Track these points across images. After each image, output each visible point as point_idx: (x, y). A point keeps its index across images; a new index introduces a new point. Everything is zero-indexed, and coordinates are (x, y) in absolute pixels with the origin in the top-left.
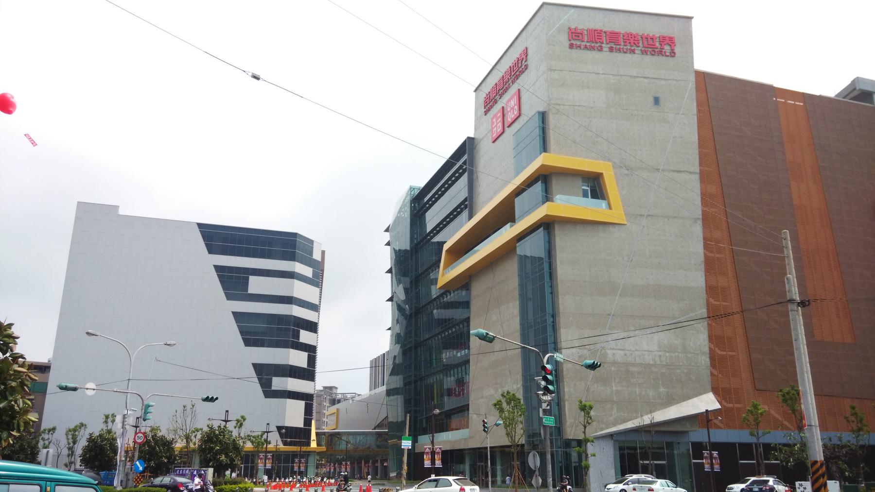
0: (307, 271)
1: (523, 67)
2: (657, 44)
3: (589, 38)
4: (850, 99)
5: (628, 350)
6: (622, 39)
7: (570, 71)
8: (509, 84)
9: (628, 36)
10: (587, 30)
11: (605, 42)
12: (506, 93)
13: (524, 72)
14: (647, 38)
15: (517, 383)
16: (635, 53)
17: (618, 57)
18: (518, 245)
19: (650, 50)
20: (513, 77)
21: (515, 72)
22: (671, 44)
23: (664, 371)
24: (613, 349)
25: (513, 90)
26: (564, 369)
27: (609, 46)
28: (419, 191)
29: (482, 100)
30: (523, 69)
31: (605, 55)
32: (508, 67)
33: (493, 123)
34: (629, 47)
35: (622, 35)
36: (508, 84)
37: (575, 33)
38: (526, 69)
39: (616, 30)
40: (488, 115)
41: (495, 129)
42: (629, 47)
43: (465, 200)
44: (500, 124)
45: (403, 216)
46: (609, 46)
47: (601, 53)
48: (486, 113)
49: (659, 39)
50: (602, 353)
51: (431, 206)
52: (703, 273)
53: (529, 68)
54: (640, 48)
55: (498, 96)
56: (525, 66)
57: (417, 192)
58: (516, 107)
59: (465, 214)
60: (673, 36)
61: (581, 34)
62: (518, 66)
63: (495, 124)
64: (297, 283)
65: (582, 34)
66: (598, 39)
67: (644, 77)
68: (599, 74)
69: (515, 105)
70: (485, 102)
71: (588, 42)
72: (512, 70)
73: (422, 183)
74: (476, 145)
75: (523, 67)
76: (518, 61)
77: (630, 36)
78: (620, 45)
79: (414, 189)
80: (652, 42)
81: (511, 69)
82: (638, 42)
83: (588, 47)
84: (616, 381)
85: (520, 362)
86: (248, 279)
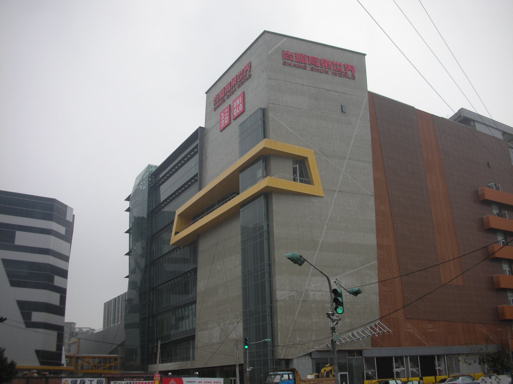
0: (62, 230)
1: (248, 75)
2: (343, 70)
3: (297, 59)
4: (458, 122)
5: (325, 292)
6: (319, 64)
7: (284, 81)
8: (235, 88)
9: (324, 62)
10: (295, 54)
11: (308, 64)
12: (233, 95)
13: (248, 79)
14: (336, 65)
15: (237, 318)
16: (328, 74)
17: (317, 75)
18: (241, 210)
19: (339, 73)
20: (239, 83)
21: (240, 79)
22: (352, 70)
23: (349, 306)
24: (314, 291)
25: (239, 92)
26: (278, 306)
27: (310, 66)
28: (155, 169)
29: (212, 99)
30: (247, 77)
31: (308, 72)
32: (235, 76)
33: (221, 117)
34: (324, 69)
35: (319, 60)
36: (234, 88)
37: (287, 55)
38: (250, 77)
39: (315, 56)
40: (217, 110)
41: (223, 121)
42: (324, 69)
43: (196, 175)
44: (227, 117)
45: (141, 188)
46: (310, 66)
47: (305, 71)
48: (215, 109)
49: (344, 66)
50: (306, 293)
51: (165, 180)
52: (375, 235)
53: (252, 77)
54: (332, 71)
55: (226, 97)
56: (249, 75)
57: (154, 170)
58: (241, 105)
59: (196, 186)
60: (354, 65)
61: (291, 55)
62: (243, 75)
63: (223, 117)
64: (53, 238)
65: (292, 56)
66: (303, 60)
67: (335, 92)
68: (304, 85)
69: (240, 103)
70: (215, 101)
71: (296, 62)
72: (238, 78)
73: (158, 163)
74: (206, 134)
75: (248, 75)
76: (243, 71)
77: (325, 62)
78: (318, 67)
79: (152, 167)
80: (339, 67)
81: (237, 77)
82: (331, 66)
83: (296, 66)
84: (315, 315)
85: (241, 301)
86: (15, 233)
